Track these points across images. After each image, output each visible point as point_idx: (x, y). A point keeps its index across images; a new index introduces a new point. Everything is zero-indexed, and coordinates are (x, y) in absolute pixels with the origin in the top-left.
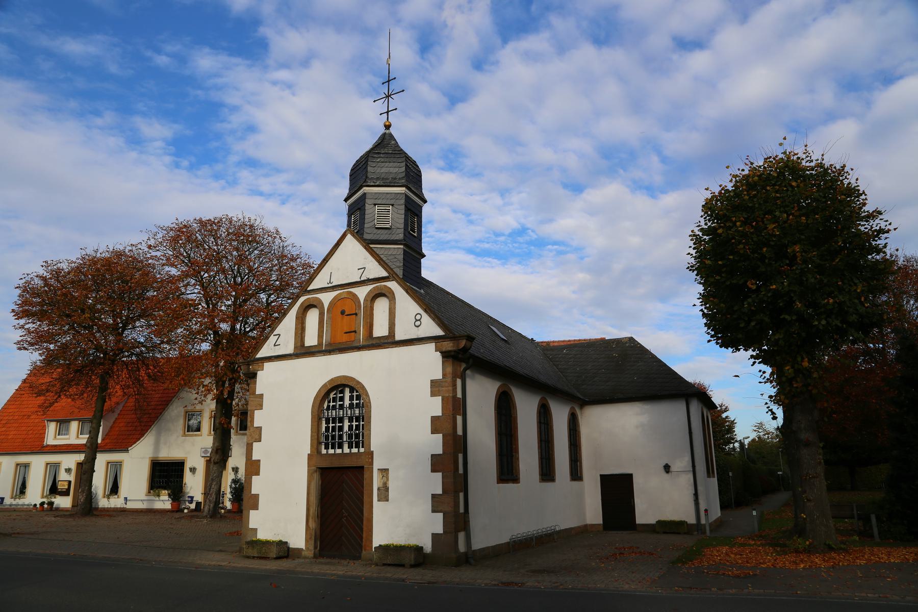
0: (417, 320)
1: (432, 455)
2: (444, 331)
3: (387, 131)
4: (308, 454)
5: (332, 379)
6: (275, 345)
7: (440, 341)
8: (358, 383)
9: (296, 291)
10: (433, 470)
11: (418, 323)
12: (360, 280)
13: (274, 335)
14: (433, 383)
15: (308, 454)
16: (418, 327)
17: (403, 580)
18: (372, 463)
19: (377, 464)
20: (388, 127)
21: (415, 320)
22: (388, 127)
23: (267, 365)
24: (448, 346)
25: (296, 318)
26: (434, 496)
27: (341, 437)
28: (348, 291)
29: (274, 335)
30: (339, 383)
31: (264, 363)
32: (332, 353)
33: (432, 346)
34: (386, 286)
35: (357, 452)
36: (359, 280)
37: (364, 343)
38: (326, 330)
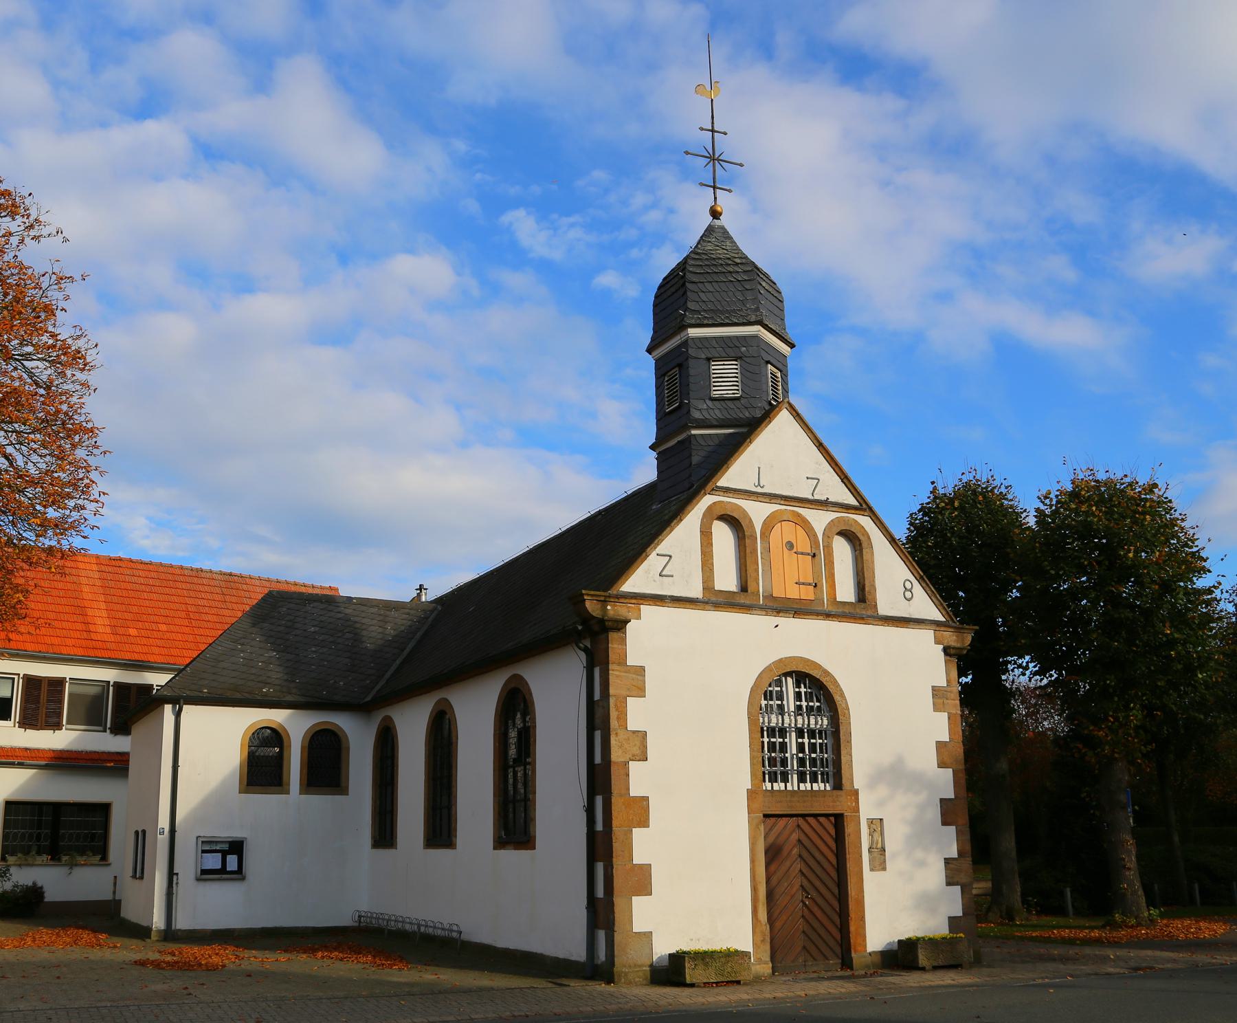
5: (780, 660)
11: (908, 594)
18: (857, 810)
37: (831, 608)
38: (763, 570)
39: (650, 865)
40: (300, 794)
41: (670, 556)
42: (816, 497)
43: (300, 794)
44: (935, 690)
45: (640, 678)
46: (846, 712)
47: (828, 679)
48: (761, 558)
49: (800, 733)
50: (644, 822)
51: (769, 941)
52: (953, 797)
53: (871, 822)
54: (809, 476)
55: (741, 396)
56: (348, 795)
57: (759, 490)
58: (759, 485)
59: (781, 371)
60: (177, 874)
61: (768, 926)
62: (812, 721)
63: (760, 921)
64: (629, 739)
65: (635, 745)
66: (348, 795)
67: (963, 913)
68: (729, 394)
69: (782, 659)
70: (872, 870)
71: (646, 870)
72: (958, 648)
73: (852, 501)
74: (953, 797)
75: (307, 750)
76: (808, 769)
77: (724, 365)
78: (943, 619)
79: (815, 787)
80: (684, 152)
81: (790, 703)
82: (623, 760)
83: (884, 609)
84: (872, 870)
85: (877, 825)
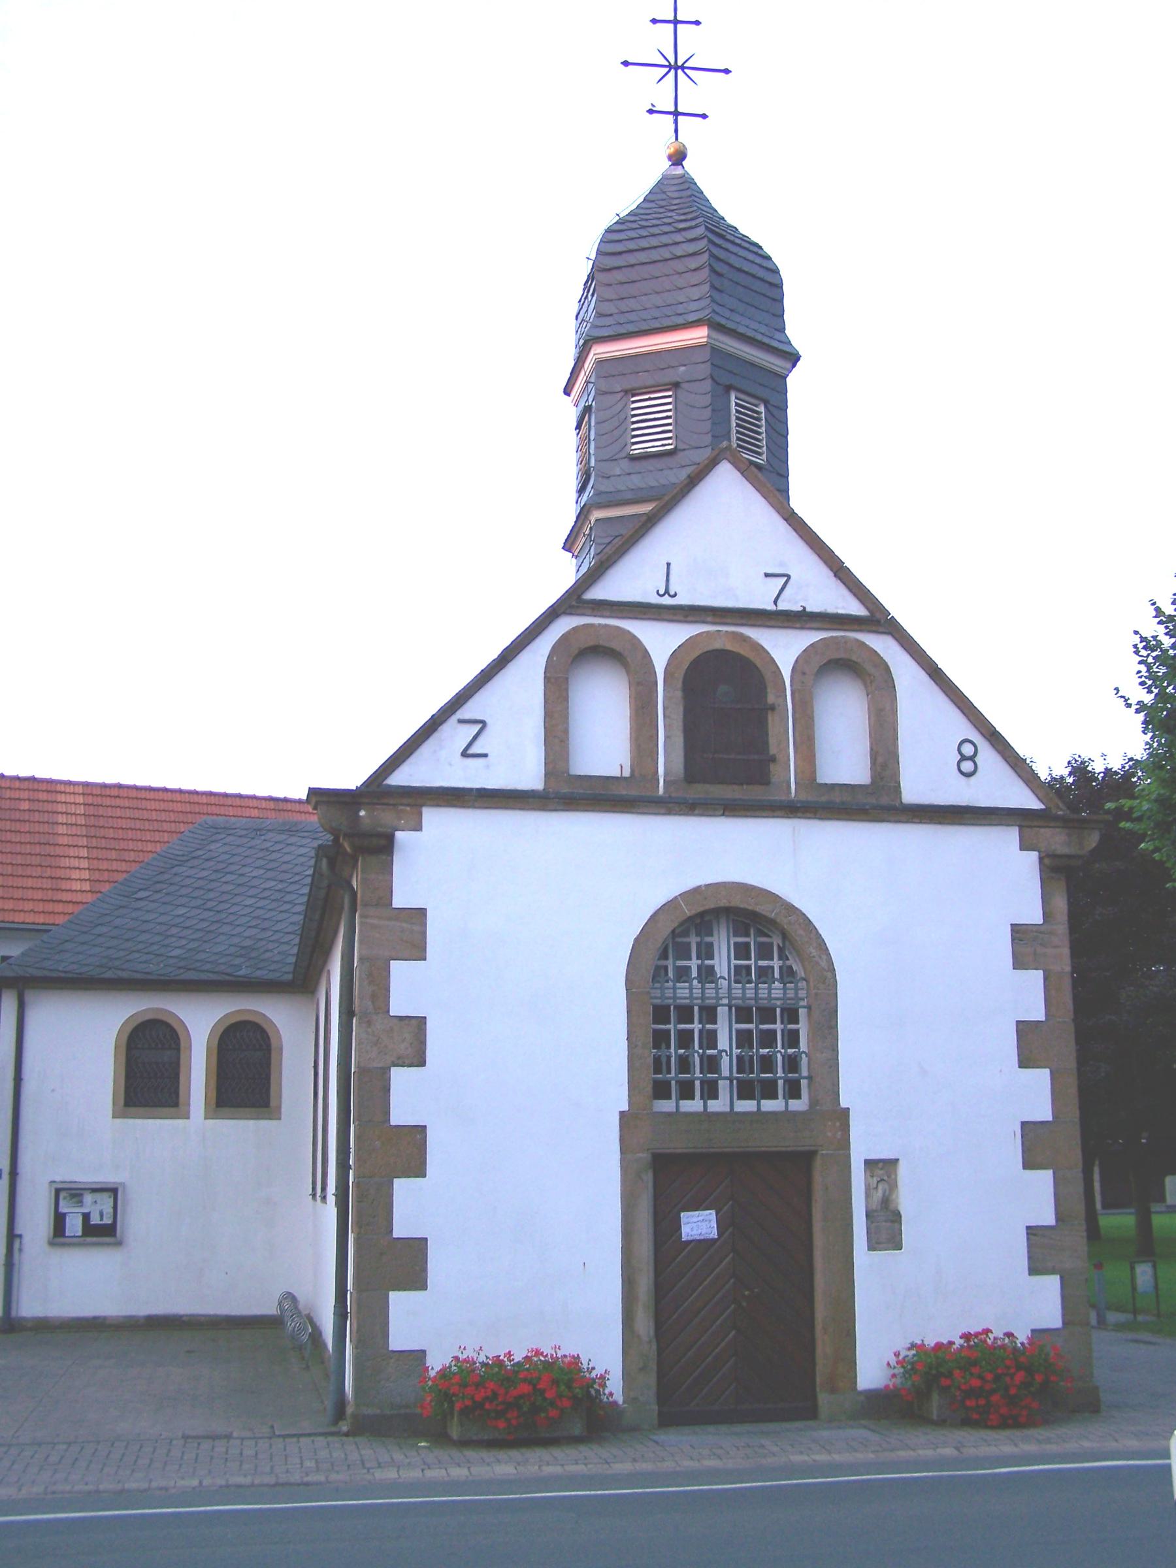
0: (963, 758)
1: (1024, 1124)
2: (389, 786)
3: (678, 171)
4: (622, 1114)
5: (696, 891)
6: (465, 754)
7: (1035, 823)
8: (791, 909)
9: (1164, 619)
10: (1028, 1164)
11: (967, 766)
12: (773, 608)
13: (461, 721)
14: (1017, 932)
15: (622, 1114)
16: (968, 775)
17: (166, 1489)
18: (844, 1144)
19: (861, 1148)
20: (678, 157)
21: (976, 759)
22: (678, 157)
23: (432, 817)
24: (1057, 840)
25: (547, 679)
26: (1032, 1232)
27: (712, 1064)
28: (733, 633)
29: (461, 721)
30: (723, 903)
31: (422, 806)
32: (799, 815)
33: (1011, 836)
34: (863, 643)
35: (755, 1109)
36: (770, 607)
37: (803, 797)
38: (667, 737)
39: (426, 1239)
40: (206, 1118)
41: (483, 723)
42: (783, 606)
43: (206, 1118)
44: (1018, 932)
45: (416, 928)
46: (829, 975)
47: (792, 918)
48: (665, 716)
49: (743, 1013)
50: (417, 1169)
51: (655, 1367)
52: (1050, 1119)
53: (869, 1164)
54: (672, 567)
55: (676, 447)
56: (280, 1119)
57: (667, 601)
58: (667, 592)
59: (766, 403)
60: (20, 1236)
61: (654, 1347)
62: (763, 993)
63: (639, 1336)
64: (392, 1029)
65: (404, 1040)
66: (280, 1119)
67: (1064, 1323)
68: (655, 447)
69: (700, 886)
70: (871, 1248)
71: (418, 1248)
72: (1069, 857)
73: (855, 608)
74: (1050, 1119)
75: (215, 1052)
76: (698, 1074)
77: (650, 399)
78: (385, 783)
79: (714, 1106)
80: (730, 71)
81: (722, 963)
82: (380, 1065)
83: (913, 791)
84: (871, 1248)
85: (318, 1192)
